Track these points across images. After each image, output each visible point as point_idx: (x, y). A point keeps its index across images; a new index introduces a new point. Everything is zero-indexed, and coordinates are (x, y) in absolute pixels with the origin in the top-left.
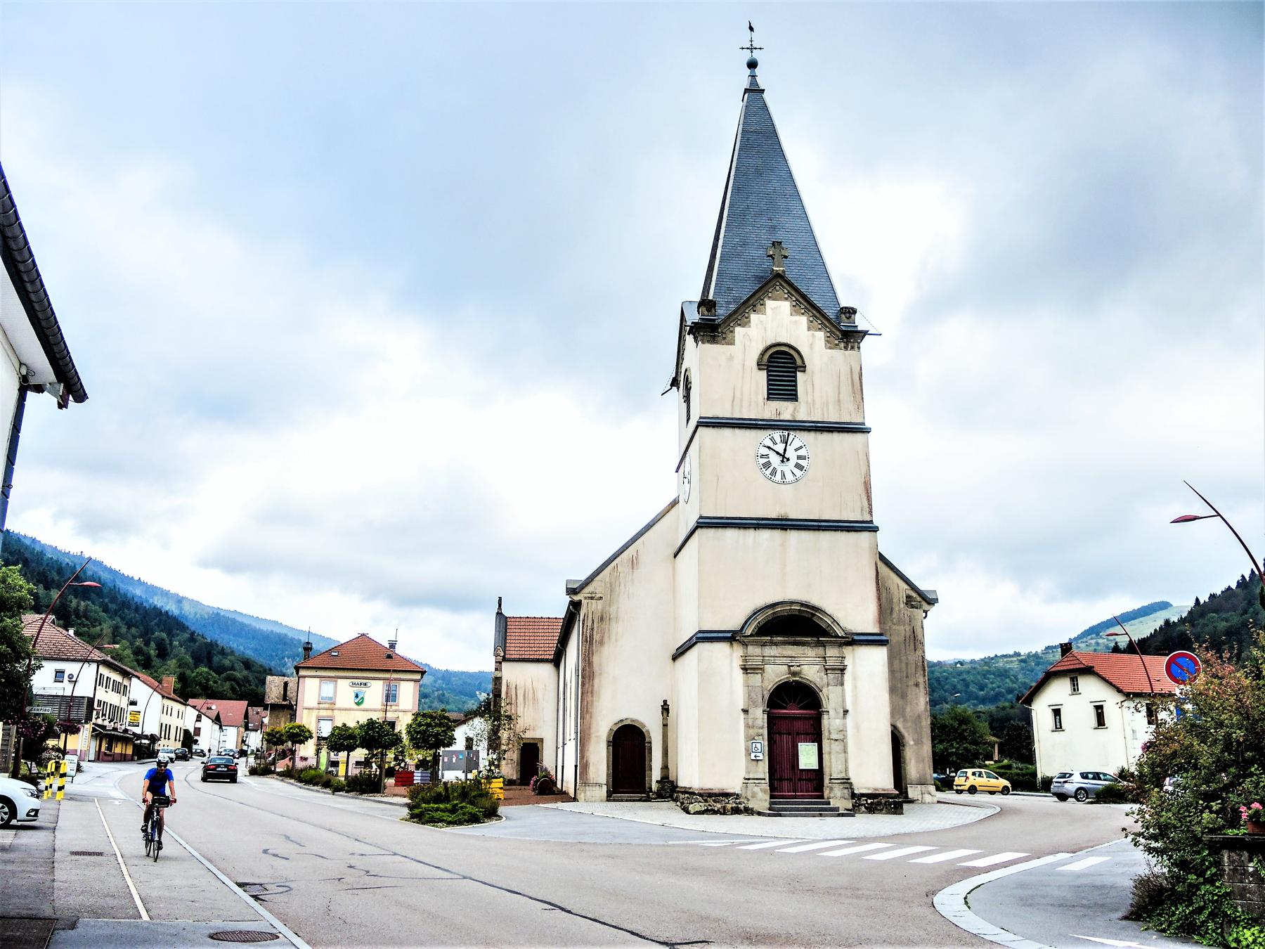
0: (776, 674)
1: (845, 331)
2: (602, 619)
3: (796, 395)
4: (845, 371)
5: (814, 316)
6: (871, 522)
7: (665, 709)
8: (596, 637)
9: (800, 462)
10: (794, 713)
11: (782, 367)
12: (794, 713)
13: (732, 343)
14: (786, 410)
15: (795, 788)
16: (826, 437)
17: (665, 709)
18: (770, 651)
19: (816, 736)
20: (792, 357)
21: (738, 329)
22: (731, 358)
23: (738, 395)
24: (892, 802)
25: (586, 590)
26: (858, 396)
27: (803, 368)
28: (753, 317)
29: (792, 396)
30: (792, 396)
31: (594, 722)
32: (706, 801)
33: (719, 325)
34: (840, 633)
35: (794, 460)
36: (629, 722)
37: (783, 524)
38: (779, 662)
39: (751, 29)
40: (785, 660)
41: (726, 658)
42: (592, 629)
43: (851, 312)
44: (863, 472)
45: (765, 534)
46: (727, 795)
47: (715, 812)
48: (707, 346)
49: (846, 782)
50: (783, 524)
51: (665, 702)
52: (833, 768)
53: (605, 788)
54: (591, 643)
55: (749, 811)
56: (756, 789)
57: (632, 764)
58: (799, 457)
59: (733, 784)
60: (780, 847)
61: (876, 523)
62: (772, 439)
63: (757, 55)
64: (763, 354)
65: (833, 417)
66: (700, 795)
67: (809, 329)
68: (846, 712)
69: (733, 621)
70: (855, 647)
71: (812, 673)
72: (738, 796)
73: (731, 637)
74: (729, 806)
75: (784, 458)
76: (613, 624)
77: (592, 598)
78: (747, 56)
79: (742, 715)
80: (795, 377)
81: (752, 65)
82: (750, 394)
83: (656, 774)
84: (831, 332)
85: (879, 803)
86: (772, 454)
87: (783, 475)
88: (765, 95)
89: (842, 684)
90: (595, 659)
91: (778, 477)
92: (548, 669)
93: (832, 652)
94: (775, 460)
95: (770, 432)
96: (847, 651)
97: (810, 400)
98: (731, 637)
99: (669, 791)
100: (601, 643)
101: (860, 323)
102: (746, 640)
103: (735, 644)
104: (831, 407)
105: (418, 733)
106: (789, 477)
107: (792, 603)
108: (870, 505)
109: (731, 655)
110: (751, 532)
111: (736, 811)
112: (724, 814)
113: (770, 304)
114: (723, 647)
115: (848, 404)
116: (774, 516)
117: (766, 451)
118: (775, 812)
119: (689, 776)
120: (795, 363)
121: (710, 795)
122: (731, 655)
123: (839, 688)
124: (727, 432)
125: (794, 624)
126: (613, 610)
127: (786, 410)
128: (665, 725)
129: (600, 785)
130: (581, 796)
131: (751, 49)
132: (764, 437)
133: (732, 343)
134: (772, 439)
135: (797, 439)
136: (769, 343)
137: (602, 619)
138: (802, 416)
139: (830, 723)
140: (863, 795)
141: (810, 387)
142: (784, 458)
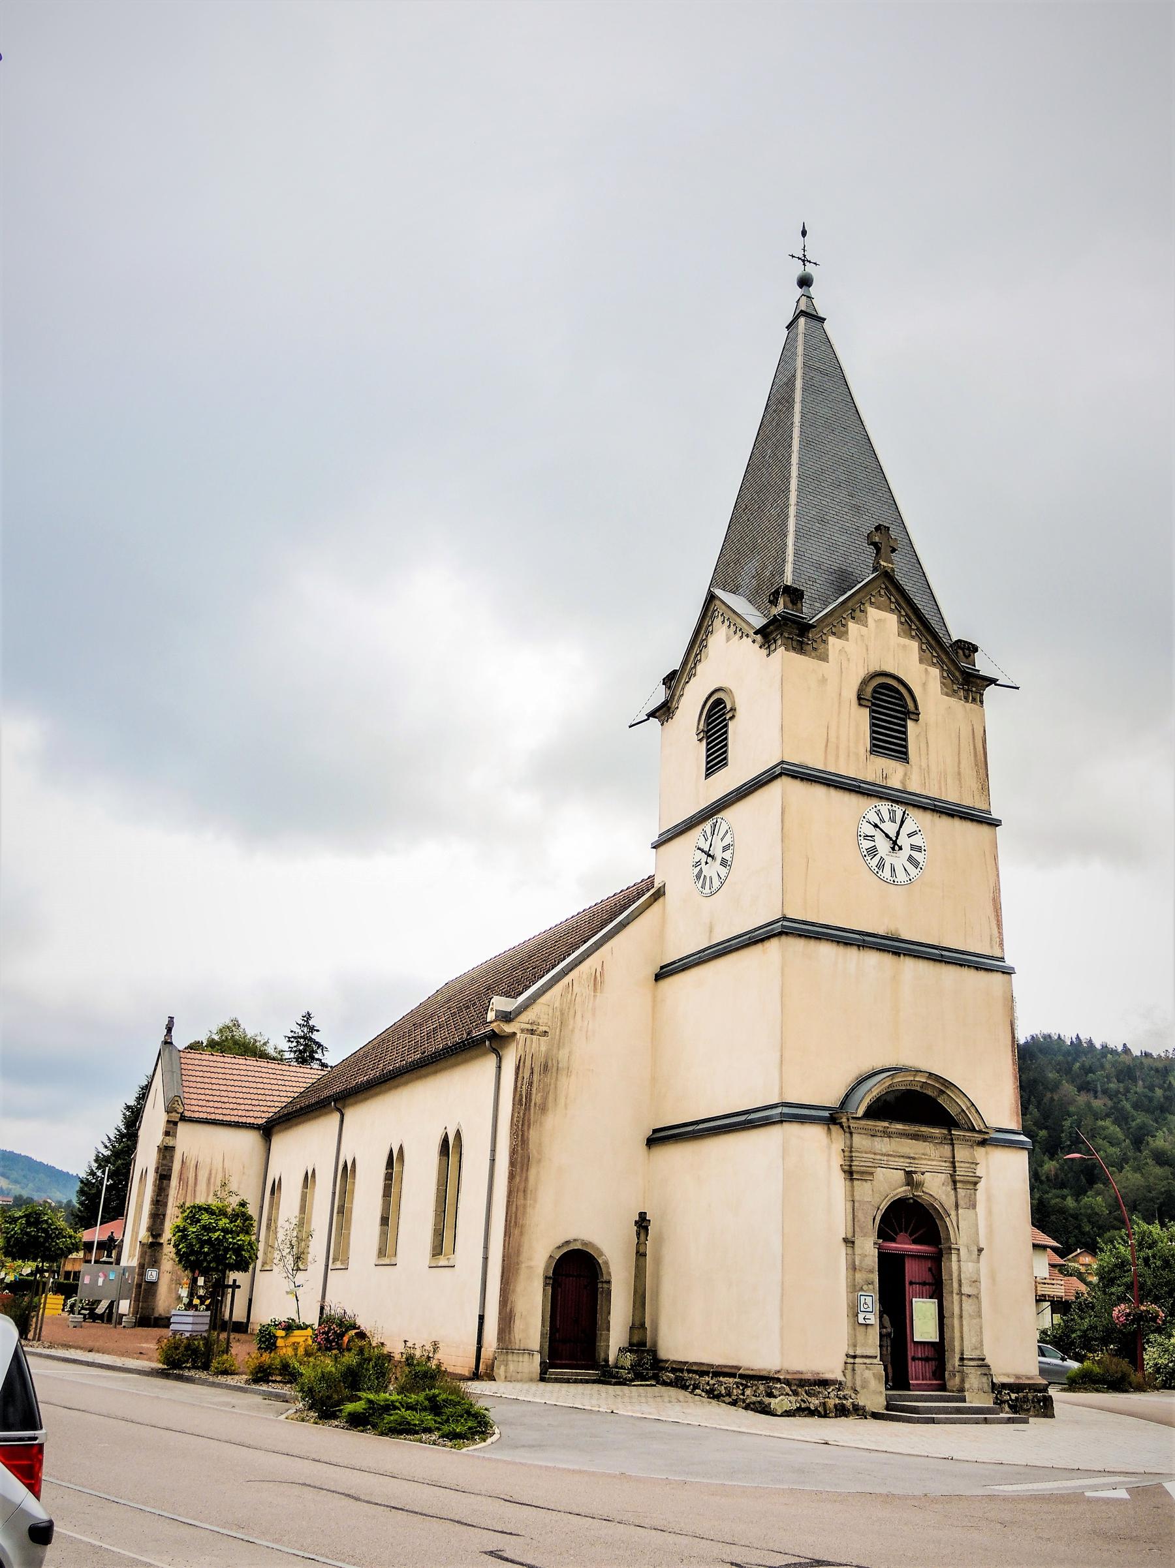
0: (887, 1185)
1: (966, 678)
2: (545, 1068)
3: (906, 753)
4: (966, 733)
5: (928, 643)
6: (1002, 959)
7: (642, 1224)
8: (536, 1098)
9: (915, 854)
10: (911, 1245)
11: (888, 709)
12: (911, 1245)
13: (824, 658)
14: (892, 773)
15: (916, 1374)
16: (945, 823)
17: (642, 1224)
18: (883, 1145)
19: (936, 1288)
20: (902, 698)
21: (832, 640)
22: (824, 680)
23: (833, 739)
24: (1024, 1401)
25: (526, 1017)
26: (982, 771)
27: (915, 715)
28: (852, 626)
29: (901, 753)
30: (901, 753)
31: (525, 1239)
32: (795, 1393)
33: (813, 626)
34: (977, 1125)
35: (907, 851)
36: (578, 1246)
37: (893, 946)
38: (902, 1160)
39: (804, 233)
40: (902, 1162)
41: (818, 1148)
42: (531, 1084)
43: (969, 649)
44: (992, 885)
45: (872, 959)
46: (824, 1383)
47: (812, 1413)
48: (793, 655)
49: (982, 1364)
50: (893, 946)
51: (642, 1216)
52: (967, 1340)
53: (537, 1358)
54: (527, 1108)
55: (859, 1412)
56: (868, 1374)
57: (582, 1320)
58: (913, 847)
59: (831, 1366)
60: (1095, 1488)
61: (1009, 962)
62: (878, 813)
63: (810, 268)
64: (865, 682)
65: (952, 796)
66: (788, 1382)
67: (921, 661)
68: (980, 1250)
69: (826, 1091)
70: (989, 1149)
71: (936, 1187)
72: (840, 1385)
73: (832, 1118)
74: (831, 1403)
75: (895, 846)
76: (563, 1081)
77: (532, 1032)
78: (798, 269)
79: (842, 1249)
80: (905, 726)
81: (805, 282)
82: (846, 741)
83: (616, 1336)
84: (949, 671)
85: (1025, 1400)
86: (879, 836)
87: (893, 870)
88: (826, 325)
89: (974, 1207)
90: (533, 1135)
91: (887, 873)
92: (249, 1141)
93: (962, 1153)
94: (883, 846)
95: (875, 802)
96: (980, 1152)
97: (924, 765)
98: (832, 1118)
99: (649, 1367)
100: (543, 1109)
101: (983, 664)
102: (853, 1124)
103: (834, 1128)
104: (949, 781)
105: (203, 1243)
106: (901, 877)
107: (918, 1071)
108: (1000, 933)
109: (829, 1148)
110: (853, 952)
111: (842, 1411)
112: (825, 1416)
113: (873, 613)
114: (815, 1134)
115: (971, 782)
116: (881, 933)
117: (870, 830)
118: (893, 1412)
119: (678, 1342)
120: (905, 706)
121: (802, 1383)
122: (829, 1148)
123: (971, 1211)
124: (820, 791)
125: (916, 1106)
126: (563, 1054)
127: (892, 773)
128: (641, 1255)
129: (530, 1353)
130: (500, 1371)
131: (804, 260)
132: (871, 809)
133: (824, 658)
134: (878, 813)
135: (916, 820)
136: (872, 670)
137: (545, 1068)
138: (914, 787)
139: (961, 1267)
140: (1004, 1386)
141: (923, 745)
142: (895, 846)
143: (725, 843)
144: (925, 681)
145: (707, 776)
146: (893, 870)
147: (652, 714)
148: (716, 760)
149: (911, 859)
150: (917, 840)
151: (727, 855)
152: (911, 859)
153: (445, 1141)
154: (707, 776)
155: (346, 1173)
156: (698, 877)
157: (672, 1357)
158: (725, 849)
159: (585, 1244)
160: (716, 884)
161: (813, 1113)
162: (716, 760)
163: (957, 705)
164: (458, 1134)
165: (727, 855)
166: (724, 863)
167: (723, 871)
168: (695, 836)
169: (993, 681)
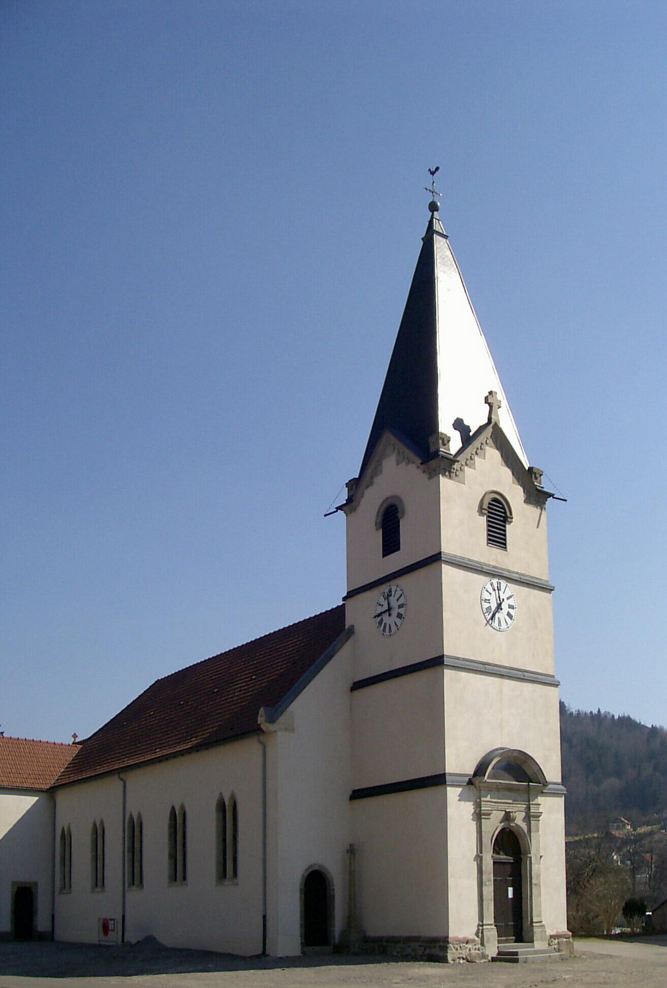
3: (505, 544)
9: (511, 611)
16: (525, 590)
36: (316, 868)
87: (500, 622)
101: (545, 484)
106: (504, 626)
120: (505, 513)
134: (492, 584)
143: (400, 602)
144: (515, 495)
145: (384, 556)
146: (500, 622)
147: (339, 508)
148: (391, 544)
149: (509, 614)
150: (511, 602)
151: (402, 611)
152: (509, 614)
153: (95, 825)
154: (384, 556)
155: (134, 831)
156: (381, 622)
157: (378, 934)
158: (400, 606)
159: (320, 866)
160: (393, 628)
161: (67, 869)
162: (391, 544)
163: (532, 511)
164: (102, 822)
165: (402, 611)
166: (400, 616)
167: (398, 621)
168: (375, 595)
169: (552, 495)
